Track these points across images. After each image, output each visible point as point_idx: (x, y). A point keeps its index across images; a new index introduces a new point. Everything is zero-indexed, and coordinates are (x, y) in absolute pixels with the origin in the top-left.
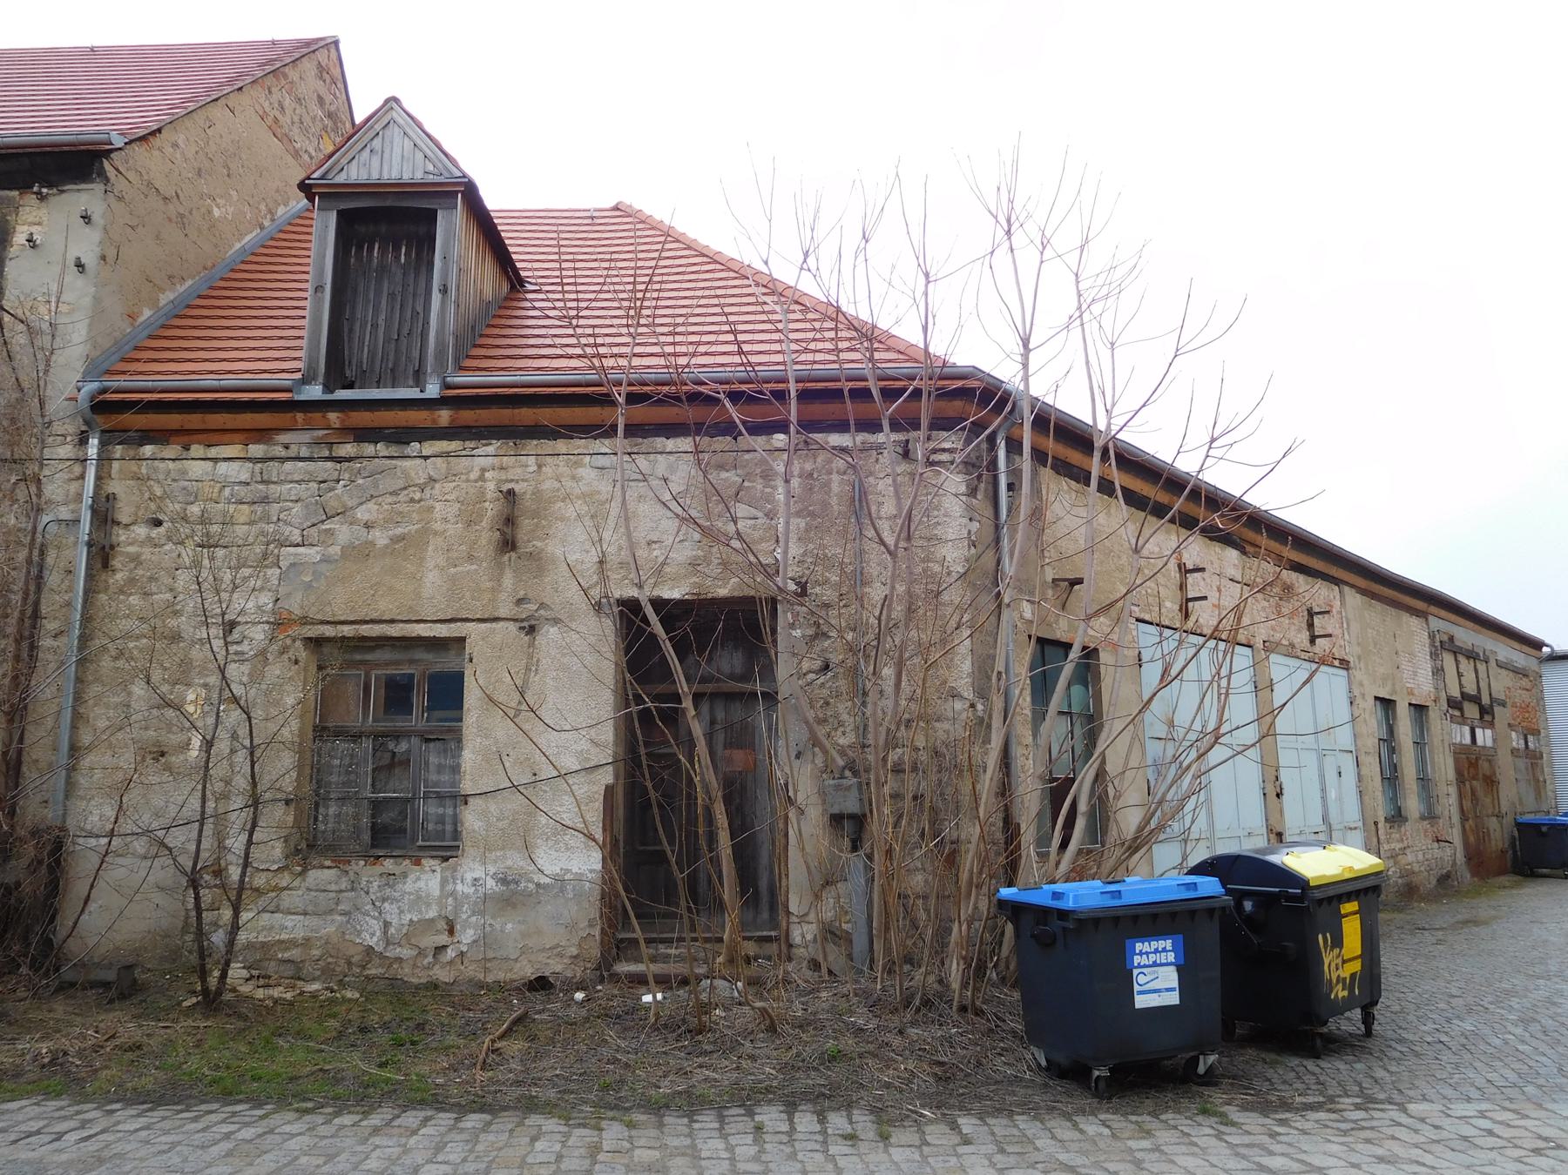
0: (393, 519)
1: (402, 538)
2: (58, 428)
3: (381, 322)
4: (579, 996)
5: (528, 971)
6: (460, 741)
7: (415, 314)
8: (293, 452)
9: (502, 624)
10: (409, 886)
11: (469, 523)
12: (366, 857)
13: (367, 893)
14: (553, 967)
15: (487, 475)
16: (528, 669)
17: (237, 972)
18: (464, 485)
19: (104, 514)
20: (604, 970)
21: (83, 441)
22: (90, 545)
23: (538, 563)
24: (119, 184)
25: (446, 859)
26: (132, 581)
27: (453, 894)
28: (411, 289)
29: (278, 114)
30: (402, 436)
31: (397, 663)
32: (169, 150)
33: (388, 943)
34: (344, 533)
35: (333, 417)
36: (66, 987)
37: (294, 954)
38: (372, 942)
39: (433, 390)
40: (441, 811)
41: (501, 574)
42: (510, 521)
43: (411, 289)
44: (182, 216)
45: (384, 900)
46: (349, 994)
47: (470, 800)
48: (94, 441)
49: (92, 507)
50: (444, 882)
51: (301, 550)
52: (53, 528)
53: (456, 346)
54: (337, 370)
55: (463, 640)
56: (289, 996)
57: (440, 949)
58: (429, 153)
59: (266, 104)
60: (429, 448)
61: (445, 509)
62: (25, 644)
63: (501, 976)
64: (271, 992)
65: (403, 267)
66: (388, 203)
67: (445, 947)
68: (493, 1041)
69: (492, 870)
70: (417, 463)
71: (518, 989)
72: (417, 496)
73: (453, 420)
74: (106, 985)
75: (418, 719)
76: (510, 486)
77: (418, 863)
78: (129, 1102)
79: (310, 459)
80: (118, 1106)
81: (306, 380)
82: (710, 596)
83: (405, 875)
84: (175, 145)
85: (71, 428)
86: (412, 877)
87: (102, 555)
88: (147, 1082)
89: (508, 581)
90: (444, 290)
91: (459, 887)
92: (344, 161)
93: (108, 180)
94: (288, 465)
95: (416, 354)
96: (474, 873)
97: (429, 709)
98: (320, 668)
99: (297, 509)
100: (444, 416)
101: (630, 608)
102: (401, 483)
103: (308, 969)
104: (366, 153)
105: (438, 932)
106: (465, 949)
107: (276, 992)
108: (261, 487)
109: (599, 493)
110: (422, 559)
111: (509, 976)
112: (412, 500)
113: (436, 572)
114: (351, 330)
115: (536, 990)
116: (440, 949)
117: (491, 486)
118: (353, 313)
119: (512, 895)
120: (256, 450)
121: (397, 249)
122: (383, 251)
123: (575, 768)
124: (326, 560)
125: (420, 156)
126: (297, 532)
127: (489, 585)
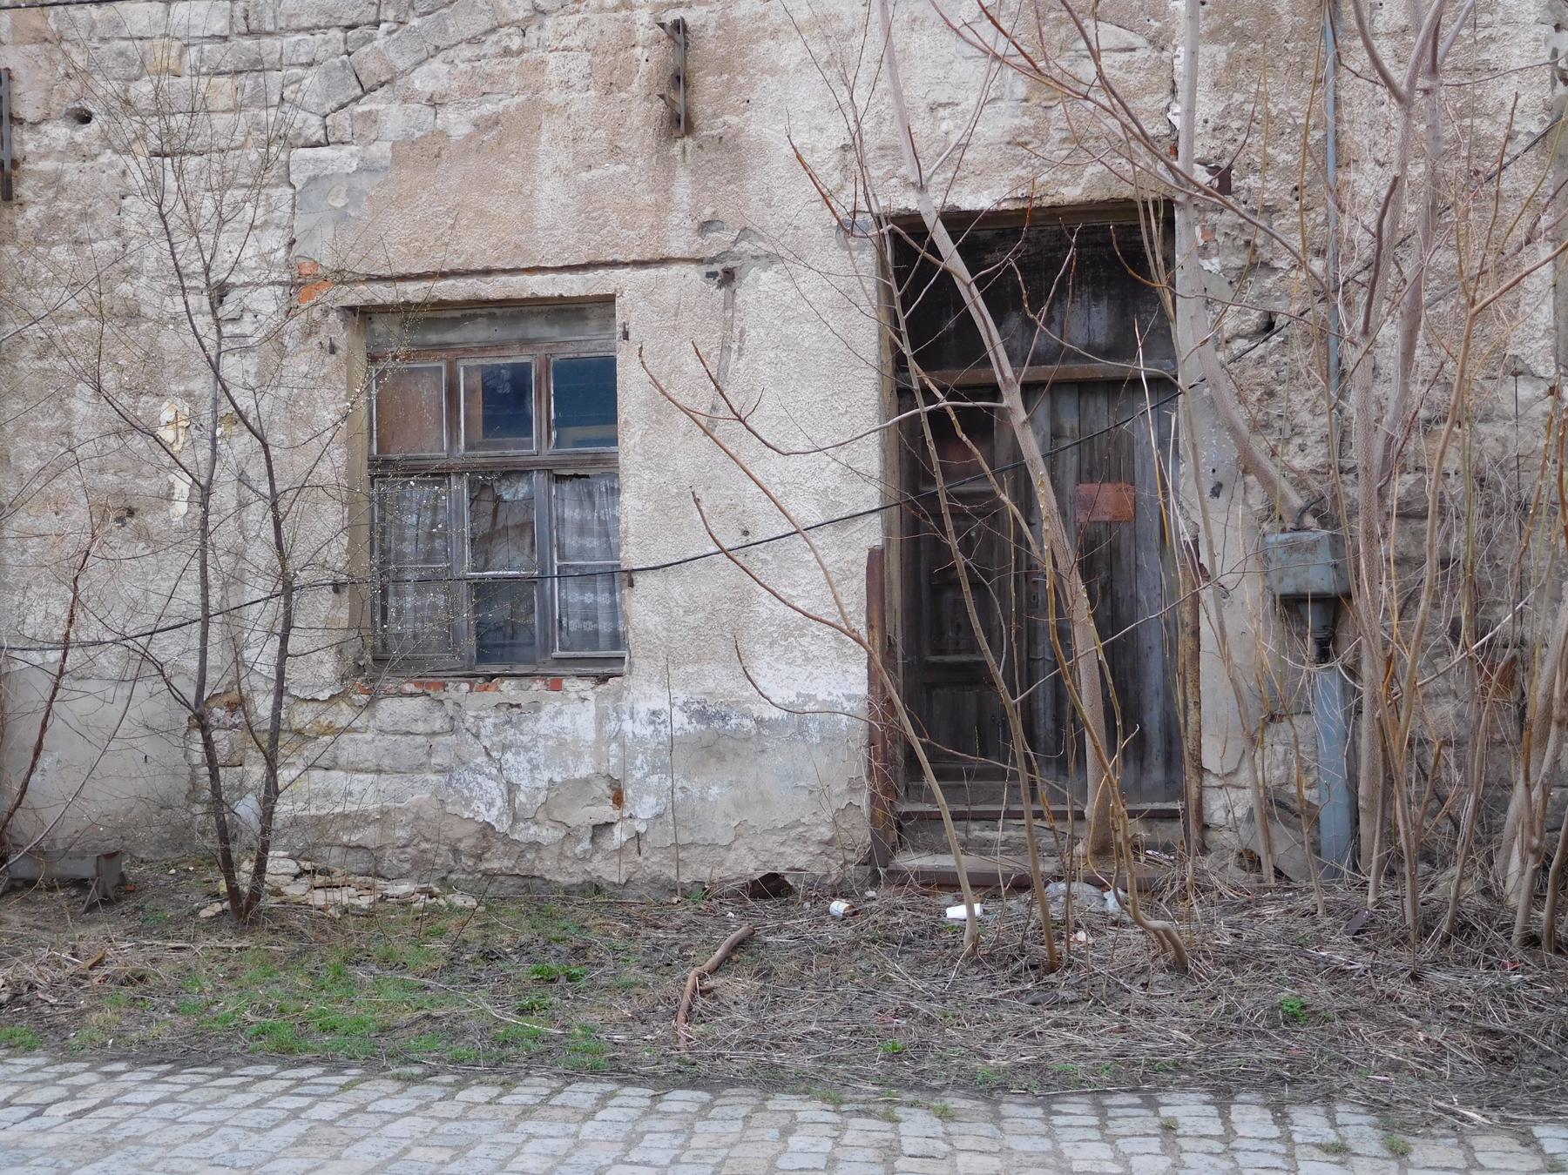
0: (476, 89)
1: (494, 121)
4: (839, 906)
5: (751, 867)
10: (544, 724)
11: (609, 88)
13: (477, 736)
14: (791, 859)
18: (595, 18)
20: (877, 865)
25: (603, 679)
26: (52, 221)
27: (618, 737)
31: (500, 346)
33: (515, 819)
34: (394, 117)
37: (368, 835)
38: (490, 816)
40: (588, 598)
41: (670, 178)
42: (680, 80)
45: (505, 748)
46: (459, 900)
47: (638, 578)
50: (601, 718)
51: (323, 152)
55: (608, 300)
56: (364, 902)
57: (601, 829)
63: (704, 873)
64: (336, 895)
67: (609, 825)
68: (702, 977)
69: (681, 697)
71: (734, 894)
72: (515, 43)
74: (82, 884)
75: (540, 444)
77: (556, 686)
80: (120, 1066)
82: (1047, 202)
83: (536, 707)
86: (548, 709)
89: (683, 190)
91: (628, 726)
96: (650, 701)
97: (560, 423)
98: (373, 359)
99: (311, 79)
102: (485, 22)
103: (390, 859)
105: (597, 801)
106: (642, 828)
107: (343, 896)
108: (248, 43)
109: (838, 18)
110: (532, 157)
111: (718, 873)
112: (507, 52)
116: (601, 829)
119: (716, 738)
124: (367, 168)
126: (315, 121)
127: (649, 199)
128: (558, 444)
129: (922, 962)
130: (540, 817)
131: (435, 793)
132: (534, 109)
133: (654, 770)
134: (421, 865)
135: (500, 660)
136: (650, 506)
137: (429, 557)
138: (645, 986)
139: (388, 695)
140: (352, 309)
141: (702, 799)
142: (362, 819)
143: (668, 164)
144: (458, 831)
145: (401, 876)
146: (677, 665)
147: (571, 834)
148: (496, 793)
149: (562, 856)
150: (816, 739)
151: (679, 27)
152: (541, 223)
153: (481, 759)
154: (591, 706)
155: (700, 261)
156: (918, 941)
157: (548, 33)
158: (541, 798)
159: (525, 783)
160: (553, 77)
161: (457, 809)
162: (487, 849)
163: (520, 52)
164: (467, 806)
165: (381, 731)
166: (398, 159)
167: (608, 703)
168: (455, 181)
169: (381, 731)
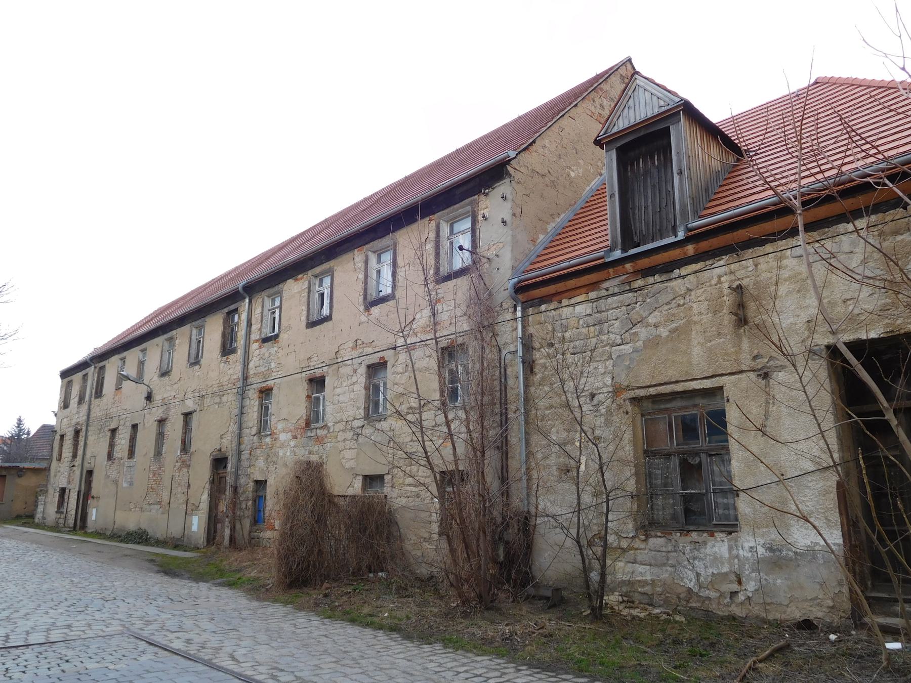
0: (670, 319)
1: (676, 329)
2: (505, 306)
3: (650, 204)
4: (833, 637)
5: (796, 613)
6: (728, 454)
7: (668, 192)
8: (610, 292)
9: (744, 375)
10: (708, 550)
11: (715, 312)
12: (681, 531)
13: (684, 553)
14: (816, 613)
15: (722, 279)
16: (767, 403)
17: (612, 599)
18: (709, 289)
19: (528, 344)
20: (856, 618)
21: (515, 307)
22: (524, 362)
23: (763, 331)
24: (517, 176)
25: (730, 533)
26: (543, 379)
27: (737, 556)
28: (663, 178)
29: (600, 111)
30: (667, 268)
31: (686, 408)
32: (541, 150)
33: (700, 587)
34: (643, 333)
35: (628, 266)
36: (530, 599)
37: (647, 589)
38: (691, 585)
39: (681, 235)
40: (725, 501)
41: (740, 341)
42: (741, 305)
43: (663, 178)
44: (553, 182)
45: (694, 559)
46: (678, 618)
47: (741, 494)
48: (519, 309)
49: (522, 343)
50: (730, 549)
51: (622, 347)
52: (509, 357)
53: (693, 204)
54: (628, 237)
55: (721, 388)
56: (642, 615)
57: (734, 594)
58: (660, 95)
59: (593, 109)
60: (684, 271)
61: (699, 307)
62: (504, 417)
63: (778, 616)
64: (632, 611)
65: (658, 167)
66: (642, 133)
67: (736, 592)
68: (755, 662)
69: (762, 542)
70: (683, 282)
71: (788, 627)
72: (682, 302)
73: (696, 250)
74: (548, 598)
75: (703, 443)
76: (738, 283)
77: (712, 535)
78: (530, 666)
79: (620, 293)
80: (524, 668)
81: (612, 249)
82: (902, 331)
83: (705, 543)
84: (544, 147)
85: (509, 304)
86: (709, 544)
87: (529, 366)
88: (545, 657)
89: (745, 345)
90: (680, 173)
91: (741, 552)
92: (615, 119)
93: (510, 175)
94: (610, 300)
95: (671, 216)
96: (751, 544)
97: (709, 435)
98: (642, 415)
99: (617, 324)
100: (690, 249)
101: (833, 351)
102: (671, 296)
103: (656, 599)
104: (626, 110)
105: (731, 582)
106: (750, 595)
107: (635, 612)
108: (597, 315)
109: (800, 274)
110: (690, 340)
111: (784, 617)
112: (679, 305)
113: (699, 347)
114: (634, 214)
115: (804, 629)
116: (734, 594)
117: (726, 285)
118: (633, 203)
119: (778, 559)
120: (593, 295)
121: (652, 158)
122: (645, 162)
123: (811, 469)
124: (635, 351)
125: (655, 99)
126: (618, 337)
127: (733, 350)
128: (709, 442)
129: (863, 668)
130: (710, 587)
131: (671, 574)
132: (689, 323)
133: (753, 571)
134: (667, 602)
135: (692, 524)
136: (743, 465)
137: (666, 485)
138: (730, 663)
139: (652, 537)
140: (633, 398)
141: (774, 584)
142: (644, 583)
143: (739, 337)
144: (680, 590)
145: (660, 606)
146: (759, 528)
147: (722, 595)
148: (692, 576)
149: (719, 604)
150: (821, 562)
151: (740, 287)
152: (694, 363)
153: (686, 563)
154: (726, 543)
155: (754, 371)
156: (867, 658)
157: (693, 297)
158: (709, 579)
159: (703, 573)
160: (695, 311)
161: (679, 581)
162: (690, 598)
163: (684, 304)
164: (682, 580)
165: (651, 550)
166: (645, 346)
167: (732, 543)
168: (664, 352)
169: (651, 550)
